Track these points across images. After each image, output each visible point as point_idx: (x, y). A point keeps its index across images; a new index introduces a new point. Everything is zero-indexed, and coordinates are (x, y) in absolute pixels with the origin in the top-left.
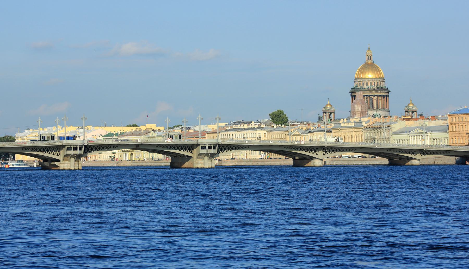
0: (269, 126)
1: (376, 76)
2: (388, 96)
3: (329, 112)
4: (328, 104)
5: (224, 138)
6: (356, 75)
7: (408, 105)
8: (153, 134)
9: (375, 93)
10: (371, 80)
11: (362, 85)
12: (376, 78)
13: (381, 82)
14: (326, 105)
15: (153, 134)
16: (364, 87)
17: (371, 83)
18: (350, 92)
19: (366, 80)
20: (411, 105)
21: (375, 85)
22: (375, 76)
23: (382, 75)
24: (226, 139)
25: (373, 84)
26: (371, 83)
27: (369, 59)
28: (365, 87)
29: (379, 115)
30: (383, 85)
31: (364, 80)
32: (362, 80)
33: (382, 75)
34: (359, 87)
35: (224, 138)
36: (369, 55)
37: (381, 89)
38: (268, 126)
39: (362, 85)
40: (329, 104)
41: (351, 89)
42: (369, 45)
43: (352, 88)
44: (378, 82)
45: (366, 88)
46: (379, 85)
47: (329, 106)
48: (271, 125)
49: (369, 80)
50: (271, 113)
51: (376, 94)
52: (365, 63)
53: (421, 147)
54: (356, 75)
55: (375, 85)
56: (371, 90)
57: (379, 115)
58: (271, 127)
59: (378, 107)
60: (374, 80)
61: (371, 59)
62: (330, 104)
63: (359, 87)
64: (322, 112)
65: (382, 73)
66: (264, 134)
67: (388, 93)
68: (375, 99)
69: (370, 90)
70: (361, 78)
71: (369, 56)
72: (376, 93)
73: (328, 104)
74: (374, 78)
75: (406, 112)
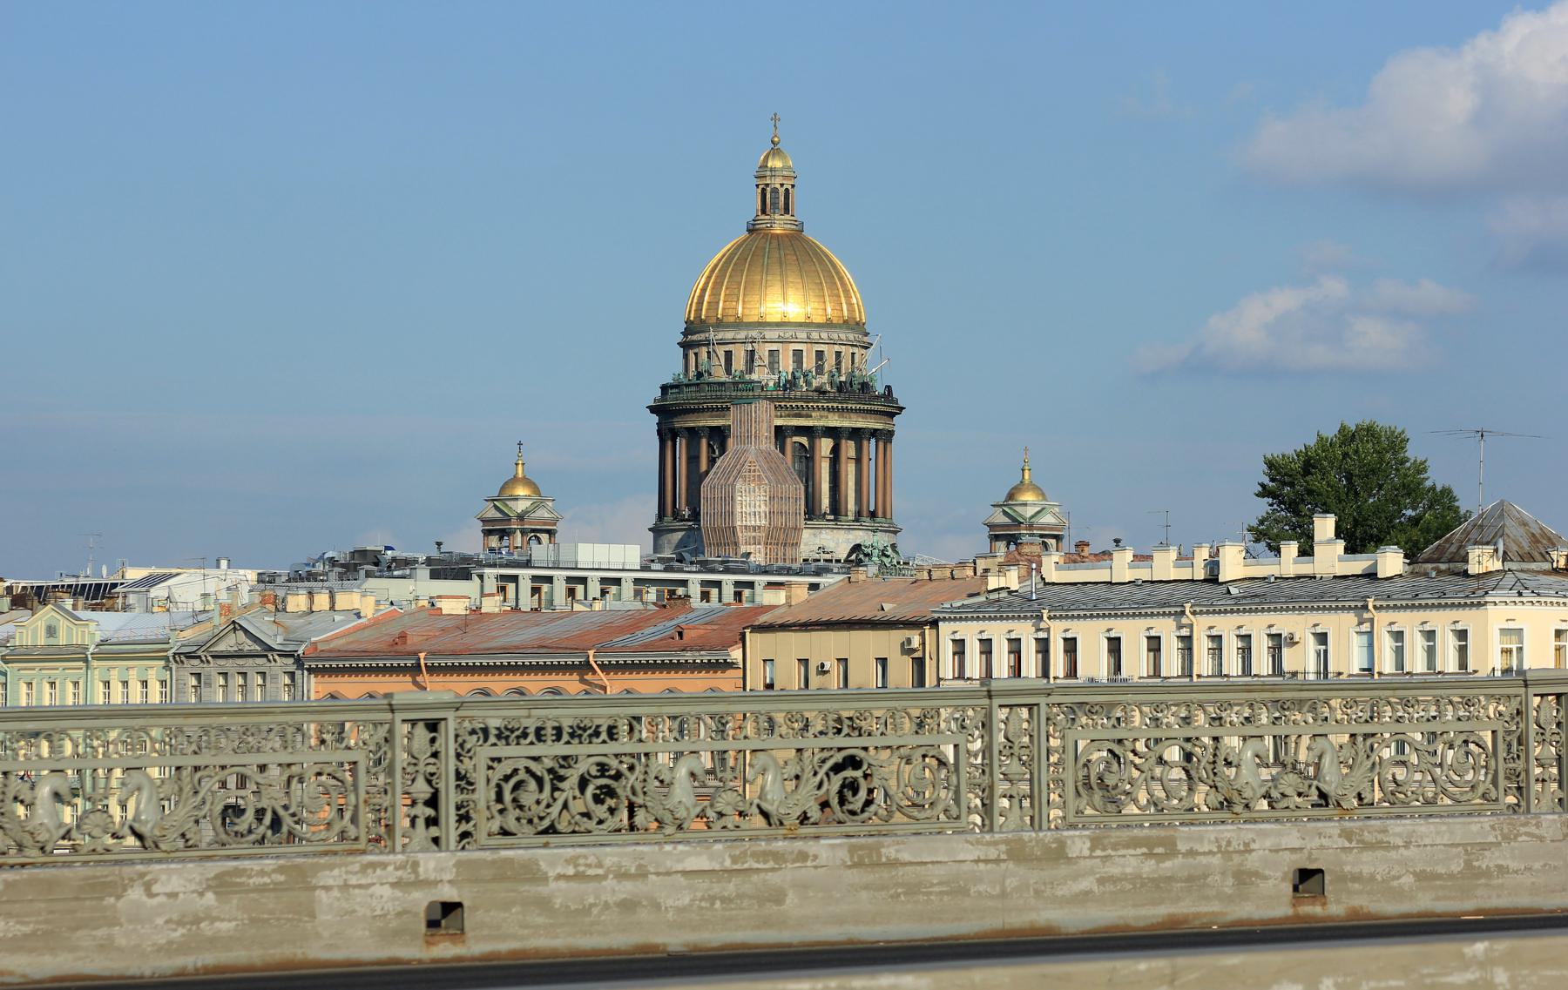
0: (1533, 566)
1: (829, 311)
2: (891, 433)
3: (523, 532)
4: (514, 480)
5: (961, 677)
6: (691, 305)
7: (1011, 496)
8: (51, 631)
9: (826, 413)
10: (802, 335)
11: (739, 364)
12: (828, 325)
13: (856, 350)
14: (503, 488)
15: (51, 631)
16: (754, 377)
17: (798, 355)
18: (653, 409)
19: (771, 334)
20: (1028, 497)
21: (820, 370)
22: (821, 312)
23: (860, 312)
24: (960, 684)
25: (809, 363)
26: (798, 355)
27: (775, 204)
28: (760, 375)
29: (890, 552)
30: (875, 368)
31: (754, 333)
32: (742, 335)
33: (860, 312)
34: (720, 375)
35: (961, 677)
36: (776, 182)
37: (854, 391)
38: (1525, 566)
39: (739, 364)
40: (524, 477)
41: (664, 388)
42: (775, 118)
43: (669, 380)
44: (837, 348)
45: (771, 384)
46: (847, 368)
47: (521, 491)
48: (1545, 557)
49: (788, 333)
50: (1291, 443)
51: (834, 421)
52: (750, 231)
53: (1032, 760)
54: (691, 305)
55: (820, 370)
56: (807, 400)
57: (890, 552)
58: (1545, 573)
59: (836, 509)
60: (815, 335)
61: (787, 210)
62: (528, 482)
63: (724, 378)
64: (479, 526)
65: (855, 289)
66: (1553, 643)
67: (892, 415)
68: (823, 454)
69: (801, 399)
70: (739, 324)
71: (775, 191)
72: (831, 415)
73: (514, 480)
74: (819, 326)
75: (996, 538)
